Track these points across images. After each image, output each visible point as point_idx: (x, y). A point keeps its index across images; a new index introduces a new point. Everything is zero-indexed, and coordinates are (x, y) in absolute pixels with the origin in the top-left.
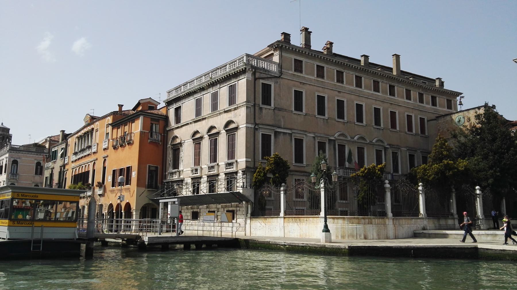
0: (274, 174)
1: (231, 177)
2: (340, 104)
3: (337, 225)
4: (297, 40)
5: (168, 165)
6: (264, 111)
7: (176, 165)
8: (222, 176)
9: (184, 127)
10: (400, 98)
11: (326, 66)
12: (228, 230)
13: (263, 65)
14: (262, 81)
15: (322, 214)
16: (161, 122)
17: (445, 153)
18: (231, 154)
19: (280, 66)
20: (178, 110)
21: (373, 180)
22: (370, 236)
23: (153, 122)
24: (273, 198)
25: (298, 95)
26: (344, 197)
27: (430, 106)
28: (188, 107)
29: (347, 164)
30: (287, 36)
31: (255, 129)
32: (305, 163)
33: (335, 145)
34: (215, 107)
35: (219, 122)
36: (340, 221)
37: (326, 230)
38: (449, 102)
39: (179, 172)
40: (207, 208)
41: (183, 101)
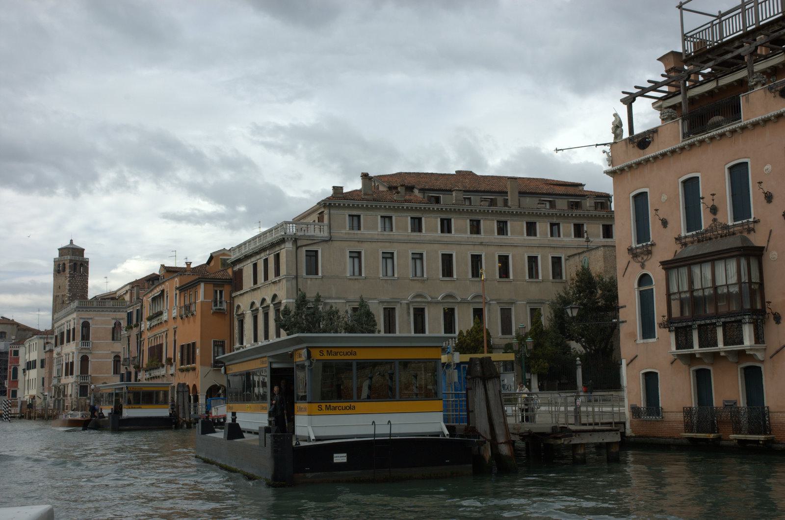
14: (304, 249)
23: (216, 289)
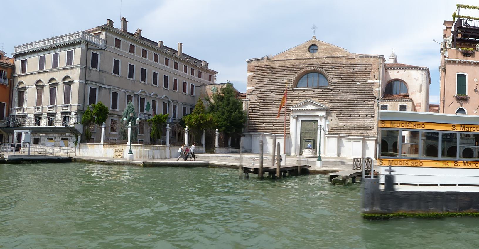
0: (98, 117)
1: (66, 116)
2: (144, 71)
3: (137, 150)
4: (118, 25)
5: (13, 102)
6: (92, 71)
7: (21, 102)
8: (59, 115)
9: (29, 76)
10: (180, 71)
11: (136, 45)
12: (64, 152)
13: (94, 40)
14: (92, 51)
15: (129, 143)
16: (8, 69)
17: (201, 109)
18: (67, 99)
19: (105, 42)
20: (24, 63)
21: (160, 123)
22: (156, 157)
24: (95, 131)
25: (117, 63)
26: (142, 132)
27: (198, 78)
28: (33, 62)
29: (145, 111)
30: (111, 22)
31: (86, 84)
32: (118, 109)
33: (138, 98)
34: (55, 64)
35: (59, 76)
36: (139, 148)
37: (131, 153)
38: (210, 76)
39: (24, 109)
40: (46, 136)
41: (29, 56)
